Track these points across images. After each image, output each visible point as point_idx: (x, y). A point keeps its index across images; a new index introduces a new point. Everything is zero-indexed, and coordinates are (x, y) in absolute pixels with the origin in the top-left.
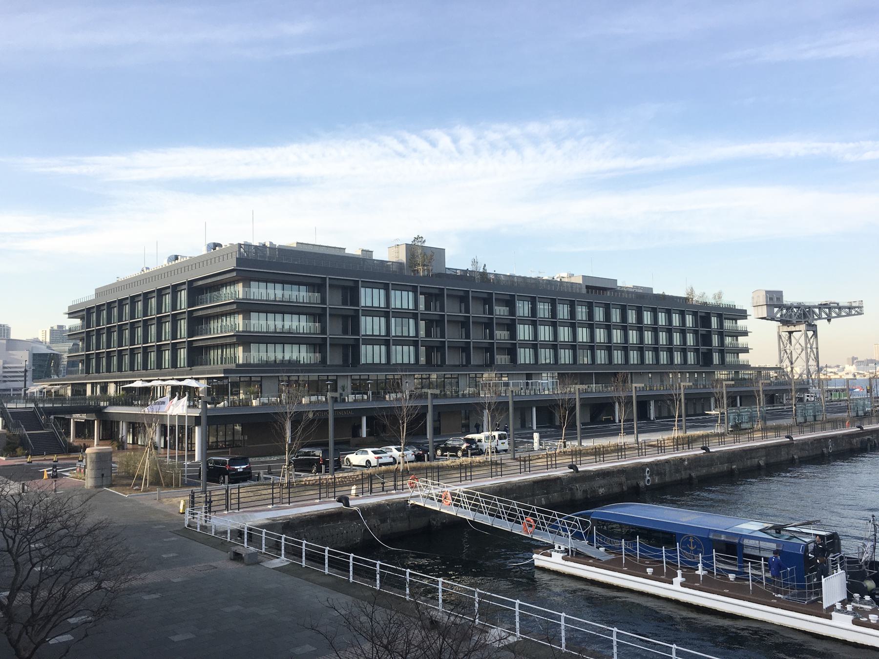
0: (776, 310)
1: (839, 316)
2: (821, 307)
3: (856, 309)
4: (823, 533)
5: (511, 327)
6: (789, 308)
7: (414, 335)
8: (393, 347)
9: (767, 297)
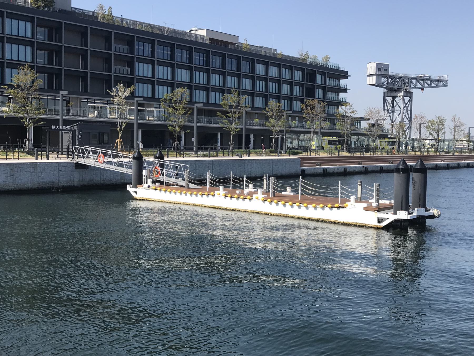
0: (383, 79)
1: (430, 86)
2: (418, 79)
3: (443, 82)
4: (378, 354)
5: (131, 64)
6: (393, 78)
7: (31, 61)
8: (157, 87)
9: (377, 67)
